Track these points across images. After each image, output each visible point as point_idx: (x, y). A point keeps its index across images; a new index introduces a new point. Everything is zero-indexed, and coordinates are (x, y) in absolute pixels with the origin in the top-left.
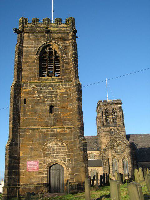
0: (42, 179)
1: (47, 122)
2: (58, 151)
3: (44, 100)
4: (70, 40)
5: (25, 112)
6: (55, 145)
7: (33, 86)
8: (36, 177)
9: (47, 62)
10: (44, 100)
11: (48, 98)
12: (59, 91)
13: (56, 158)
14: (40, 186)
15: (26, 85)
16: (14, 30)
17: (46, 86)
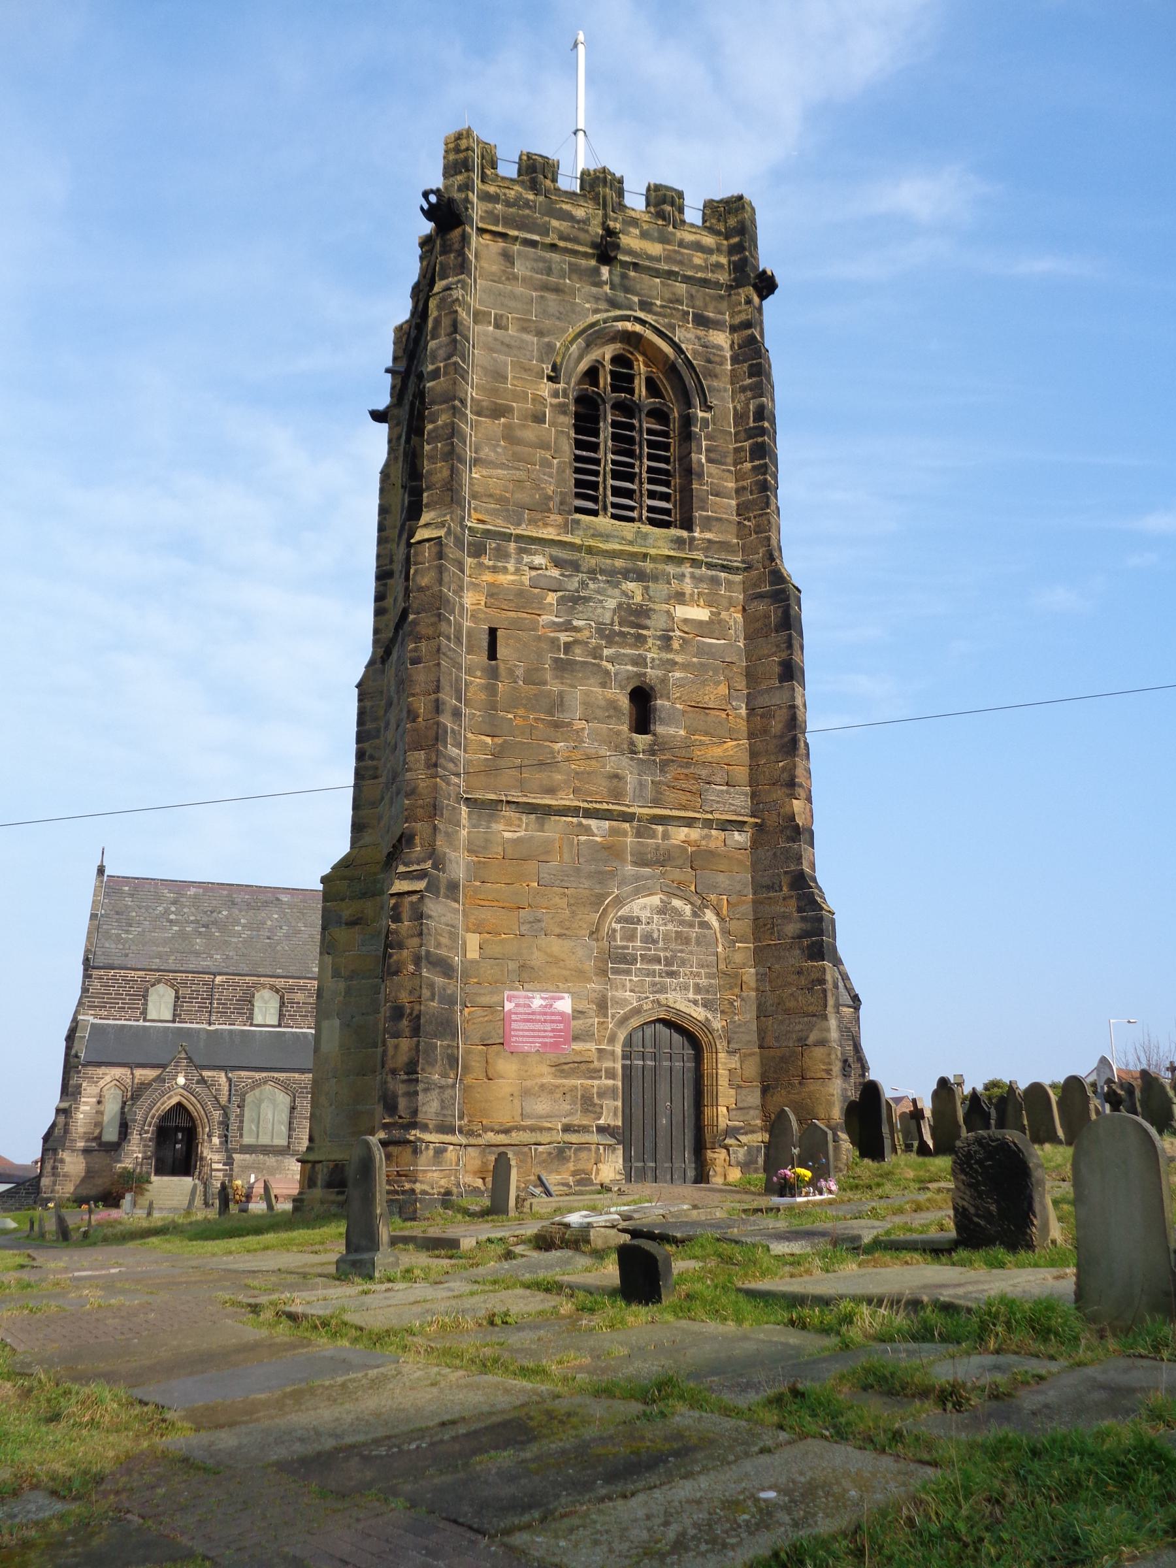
0: (591, 1099)
1: (615, 781)
8: (557, 1087)
9: (645, 468)
10: (596, 653)
11: (622, 645)
12: (683, 612)
13: (663, 989)
14: (573, 1138)
15: (498, 549)
17: (611, 573)
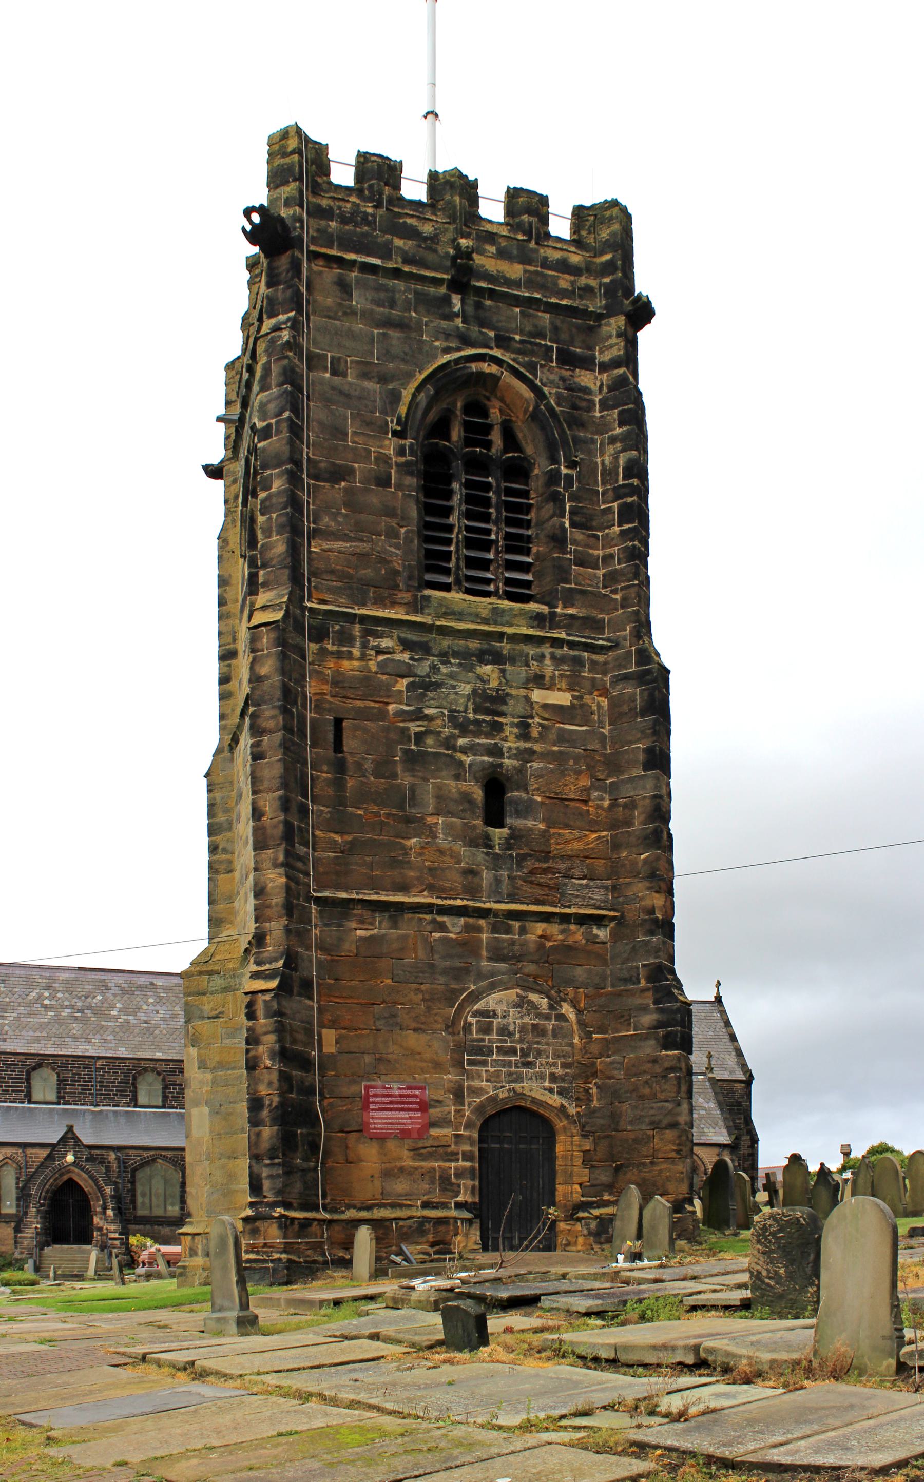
1: (470, 877)
3: (449, 743)
4: (604, 367)
5: (339, 801)
6: (517, 1006)
7: (386, 643)
8: (416, 1169)
11: (477, 734)
13: (519, 1079)
15: (341, 632)
16: (248, 212)
17: (464, 655)
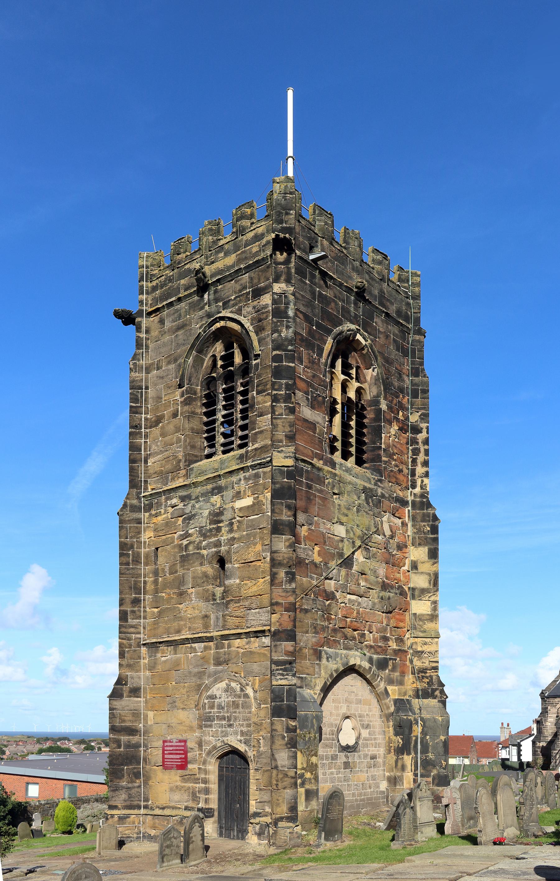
2: (241, 710)
13: (226, 735)
